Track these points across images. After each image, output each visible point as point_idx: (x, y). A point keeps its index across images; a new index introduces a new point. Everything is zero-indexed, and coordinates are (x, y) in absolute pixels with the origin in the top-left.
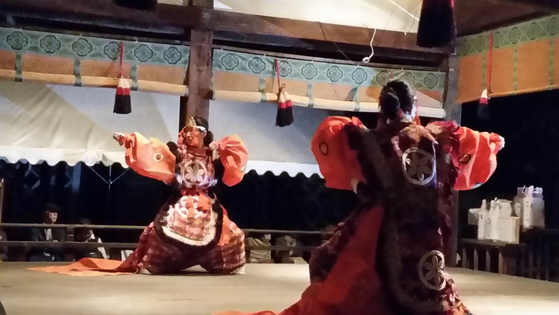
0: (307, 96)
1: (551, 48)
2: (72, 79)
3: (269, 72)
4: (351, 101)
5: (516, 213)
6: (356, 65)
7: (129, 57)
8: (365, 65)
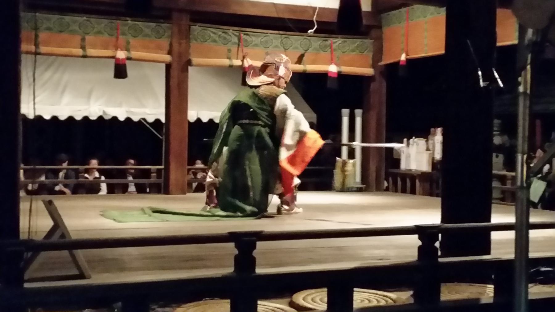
2: (80, 52)
7: (124, 34)
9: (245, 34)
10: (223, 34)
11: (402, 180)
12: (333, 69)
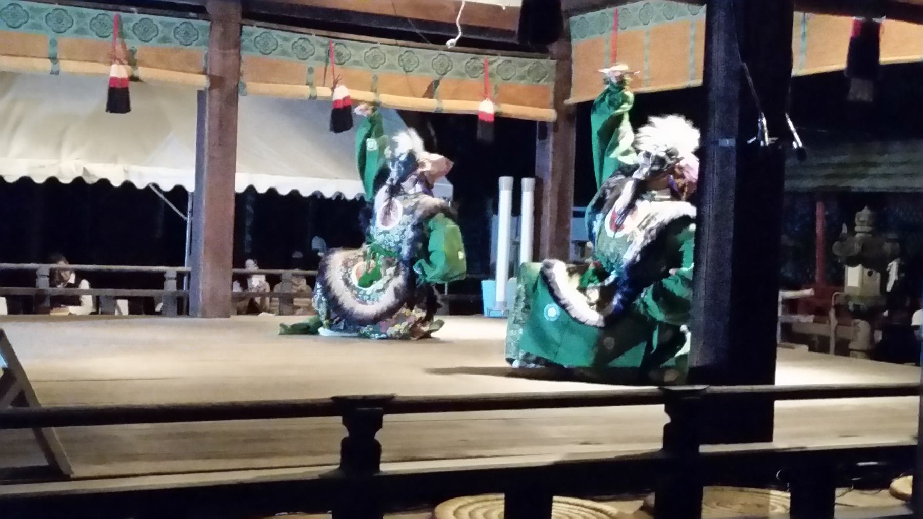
0: (372, 91)
2: (48, 65)
3: (318, 59)
4: (431, 97)
6: (197, 19)
8: (450, 50)
12: (487, 108)
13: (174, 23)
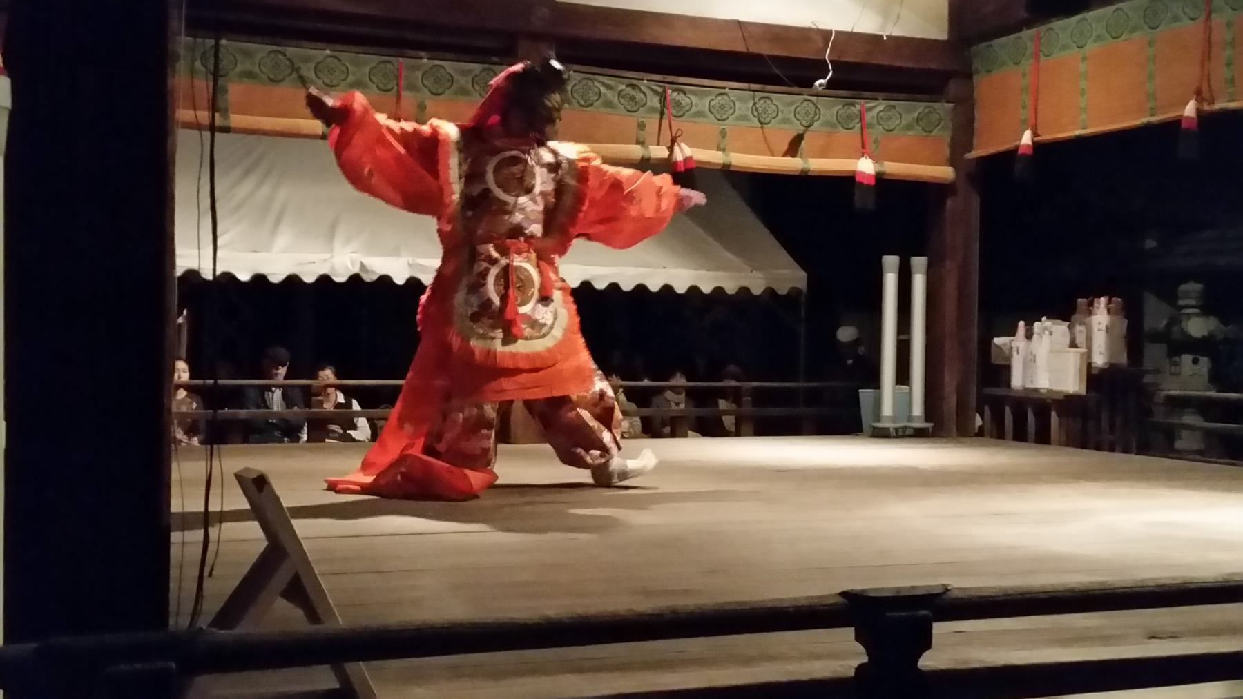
0: (719, 149)
1: (1150, 51)
4: (794, 156)
5: (1078, 341)
7: (412, 87)
8: (817, 95)
9: (674, 90)
10: (629, 89)
11: (1015, 414)
12: (866, 166)
13: (470, 71)
